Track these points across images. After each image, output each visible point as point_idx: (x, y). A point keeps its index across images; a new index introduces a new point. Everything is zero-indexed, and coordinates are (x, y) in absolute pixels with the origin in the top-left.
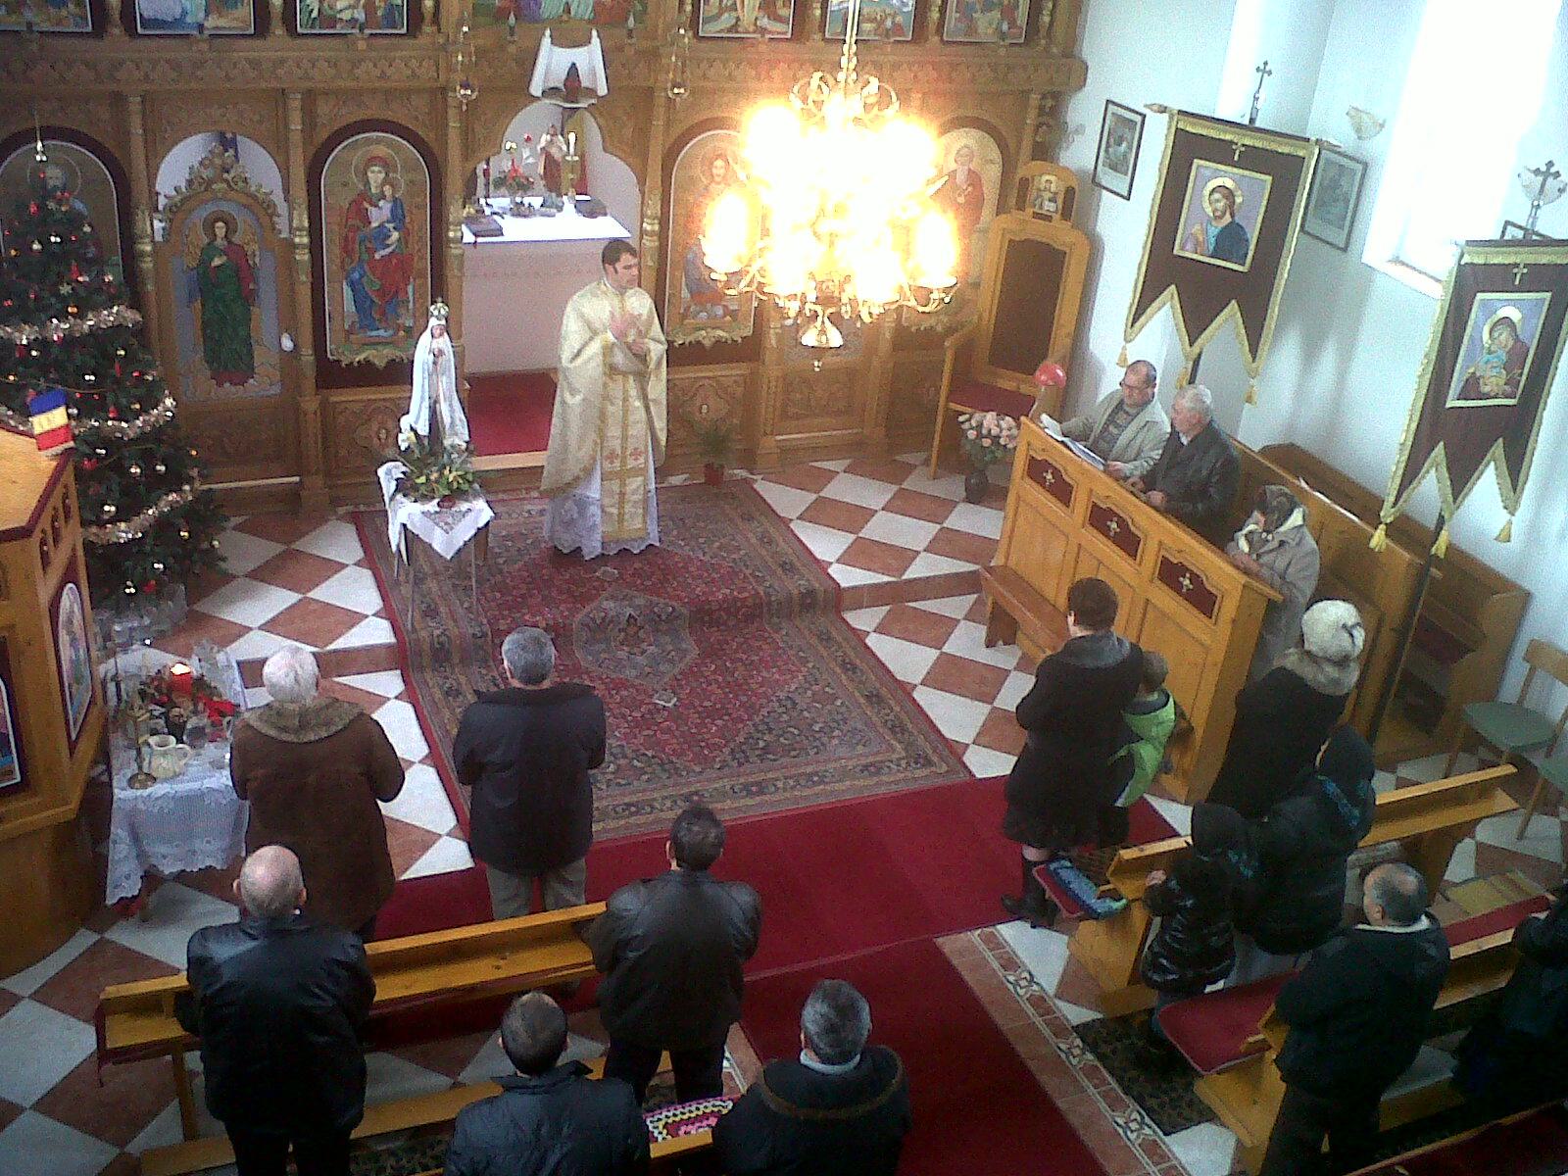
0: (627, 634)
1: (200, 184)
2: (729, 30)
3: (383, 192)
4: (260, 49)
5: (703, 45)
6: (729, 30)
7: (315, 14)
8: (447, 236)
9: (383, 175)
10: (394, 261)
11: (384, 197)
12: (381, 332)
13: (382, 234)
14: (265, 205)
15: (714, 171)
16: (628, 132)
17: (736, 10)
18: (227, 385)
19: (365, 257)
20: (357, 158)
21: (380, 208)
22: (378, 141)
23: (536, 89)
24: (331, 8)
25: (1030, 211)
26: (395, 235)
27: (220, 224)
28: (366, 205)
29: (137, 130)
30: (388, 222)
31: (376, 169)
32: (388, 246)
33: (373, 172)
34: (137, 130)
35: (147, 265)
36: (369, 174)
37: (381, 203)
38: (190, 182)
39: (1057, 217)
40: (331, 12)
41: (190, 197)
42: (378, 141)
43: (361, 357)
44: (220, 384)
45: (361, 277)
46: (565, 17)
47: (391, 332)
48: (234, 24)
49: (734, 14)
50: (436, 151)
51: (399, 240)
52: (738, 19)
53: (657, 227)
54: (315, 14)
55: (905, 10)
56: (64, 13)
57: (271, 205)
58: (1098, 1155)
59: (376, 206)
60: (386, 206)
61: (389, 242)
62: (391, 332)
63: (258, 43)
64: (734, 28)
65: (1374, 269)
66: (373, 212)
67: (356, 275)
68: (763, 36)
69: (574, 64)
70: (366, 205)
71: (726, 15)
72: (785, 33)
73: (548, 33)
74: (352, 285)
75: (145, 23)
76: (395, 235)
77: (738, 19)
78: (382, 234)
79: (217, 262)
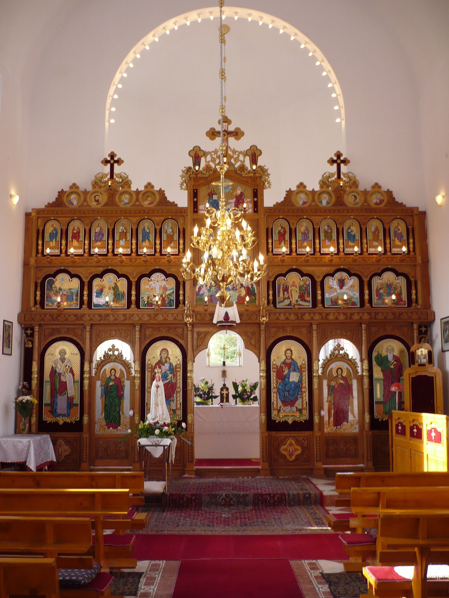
0: (226, 502)
1: (107, 357)
2: (288, 305)
3: (166, 360)
4: (129, 311)
6: (288, 305)
10: (170, 385)
11: (166, 362)
16: (253, 342)
18: (111, 428)
25: (417, 364)
29: (88, 336)
30: (168, 371)
31: (164, 352)
35: (315, 381)
38: (104, 356)
39: (427, 364)
40: (151, 302)
44: (109, 428)
48: (121, 306)
49: (289, 300)
50: (184, 347)
52: (291, 302)
54: (146, 302)
55: (355, 296)
56: (72, 303)
58: (298, 577)
59: (164, 365)
61: (168, 378)
64: (290, 304)
65: (221, 26)
75: (95, 305)
76: (170, 376)
77: (291, 302)
79: (111, 384)
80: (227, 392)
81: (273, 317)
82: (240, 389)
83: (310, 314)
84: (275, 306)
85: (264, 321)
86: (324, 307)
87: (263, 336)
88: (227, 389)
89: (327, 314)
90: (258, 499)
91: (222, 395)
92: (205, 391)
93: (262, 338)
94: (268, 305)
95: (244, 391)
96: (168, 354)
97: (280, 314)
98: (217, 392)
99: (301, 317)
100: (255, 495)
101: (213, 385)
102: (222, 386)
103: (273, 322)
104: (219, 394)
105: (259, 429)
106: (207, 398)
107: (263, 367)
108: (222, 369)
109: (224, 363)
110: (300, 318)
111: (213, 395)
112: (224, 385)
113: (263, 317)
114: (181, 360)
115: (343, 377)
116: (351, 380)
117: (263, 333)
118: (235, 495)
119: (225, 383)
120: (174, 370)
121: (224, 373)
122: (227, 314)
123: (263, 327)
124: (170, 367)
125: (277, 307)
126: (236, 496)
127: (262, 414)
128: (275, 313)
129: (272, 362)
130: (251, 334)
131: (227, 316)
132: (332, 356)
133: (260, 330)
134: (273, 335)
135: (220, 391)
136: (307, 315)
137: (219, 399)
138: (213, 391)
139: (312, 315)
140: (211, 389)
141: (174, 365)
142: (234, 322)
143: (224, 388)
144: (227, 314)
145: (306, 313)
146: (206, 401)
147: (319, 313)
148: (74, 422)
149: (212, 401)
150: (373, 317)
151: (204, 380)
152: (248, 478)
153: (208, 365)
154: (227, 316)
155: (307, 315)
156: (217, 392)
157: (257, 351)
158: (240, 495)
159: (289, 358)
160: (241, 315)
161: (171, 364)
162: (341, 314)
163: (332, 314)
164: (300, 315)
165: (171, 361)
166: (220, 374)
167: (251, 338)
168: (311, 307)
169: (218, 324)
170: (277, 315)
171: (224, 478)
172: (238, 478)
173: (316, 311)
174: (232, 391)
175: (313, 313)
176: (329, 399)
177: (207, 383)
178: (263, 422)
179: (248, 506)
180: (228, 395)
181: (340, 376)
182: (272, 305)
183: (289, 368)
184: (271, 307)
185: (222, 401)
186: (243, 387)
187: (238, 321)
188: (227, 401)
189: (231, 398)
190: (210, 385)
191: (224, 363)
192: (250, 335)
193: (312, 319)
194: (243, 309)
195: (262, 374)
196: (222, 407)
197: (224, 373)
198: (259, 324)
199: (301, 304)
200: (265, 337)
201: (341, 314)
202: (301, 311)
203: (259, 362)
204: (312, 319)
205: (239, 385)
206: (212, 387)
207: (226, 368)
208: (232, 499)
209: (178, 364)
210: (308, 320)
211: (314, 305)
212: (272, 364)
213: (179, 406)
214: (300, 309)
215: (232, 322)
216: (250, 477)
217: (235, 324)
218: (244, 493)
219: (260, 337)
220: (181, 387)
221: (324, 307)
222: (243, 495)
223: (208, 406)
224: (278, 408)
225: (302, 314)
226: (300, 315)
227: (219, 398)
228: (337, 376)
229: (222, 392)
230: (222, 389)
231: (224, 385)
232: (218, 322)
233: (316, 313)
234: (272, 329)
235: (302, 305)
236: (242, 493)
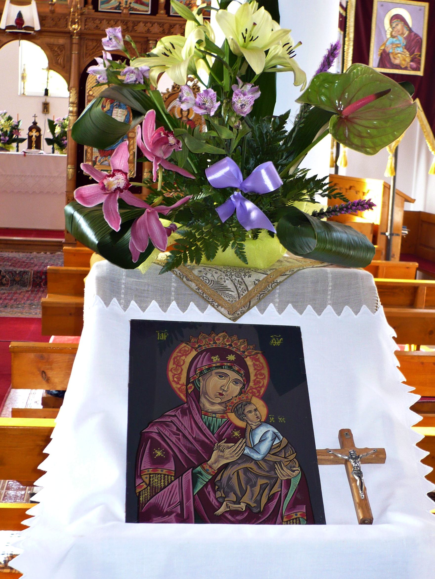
2: (115, 8)
6: (115, 8)
16: (61, 60)
41: (173, 94)
72: (147, 11)
80: (37, 134)
81: (91, 25)
82: (58, 130)
83: (145, 23)
84: (96, 8)
85: (74, 29)
86: (169, 15)
87: (75, 53)
88: (39, 130)
89: (171, 26)
90: (41, 278)
91: (30, 137)
92: (5, 130)
93: (73, 55)
94: (85, 6)
95: (64, 133)
97: (101, 20)
98: (24, 134)
99: (133, 27)
100: (36, 273)
101: (19, 122)
102: (32, 124)
103: (90, 32)
104: (26, 137)
105: (65, 186)
106: (8, 141)
107: (74, 98)
108: (43, 100)
109: (46, 91)
110: (130, 29)
111: (19, 137)
112: (35, 123)
113: (73, 23)
115: (189, 120)
116: (201, 124)
117: (75, 47)
118: (9, 272)
119: (37, 121)
121: (46, 107)
122: (20, 15)
123: (76, 38)
125: (100, 10)
126: (10, 272)
127: (69, 166)
128: (94, 19)
129: (87, 91)
130: (59, 48)
131: (20, 18)
132: (176, 89)
133: (72, 44)
134: (91, 52)
135: (28, 131)
136: (141, 24)
137: (26, 143)
138: (20, 131)
139: (149, 25)
140: (15, 128)
142: (32, 29)
143: (35, 127)
144: (20, 15)
145: (139, 22)
146: (7, 146)
147: (159, 24)
149: (18, 146)
150: (130, 29)
151: (5, 114)
152: (46, 253)
153: (23, 92)
154: (20, 18)
155: (141, 24)
156: (24, 134)
157: (68, 75)
158: (15, 272)
160: (42, 18)
162: (156, 24)
163: (177, 26)
164: (130, 24)
166: (40, 107)
167: (59, 55)
168: (149, 13)
169: (7, 31)
170: (98, 22)
171: (12, 252)
172: (31, 253)
173: (154, 21)
174: (47, 134)
175: (151, 22)
177: (10, 118)
178: (70, 178)
179: (26, 286)
180: (39, 138)
181: (184, 119)
182: (91, 7)
184: (89, 9)
185: (30, 147)
186: (63, 127)
187: (37, 27)
188: (38, 147)
189: (44, 143)
190: (14, 122)
191: (46, 91)
192: (56, 49)
193: (148, 31)
194: (47, 10)
195: (71, 109)
196: (25, 155)
197: (46, 107)
198: (70, 34)
199: (135, 7)
200: (79, 54)
201: (156, 24)
202: (133, 18)
203: (69, 90)
204: (148, 31)
205: (56, 125)
206: (17, 126)
207: (48, 100)
208: (4, 277)
210: (143, 33)
211: (155, 11)
212: (87, 95)
214: (133, 16)
215: (28, 28)
216: (48, 253)
217: (32, 32)
218: (22, 270)
219: (71, 54)
221: (169, 15)
222: (21, 271)
223: (8, 153)
224: (94, 159)
225: (133, 22)
226: (130, 24)
227: (26, 142)
228: (181, 118)
229: (31, 134)
230: (30, 129)
231: (35, 123)
232: (8, 27)
233: (154, 23)
234: (90, 43)
235: (136, 10)
236: (19, 270)
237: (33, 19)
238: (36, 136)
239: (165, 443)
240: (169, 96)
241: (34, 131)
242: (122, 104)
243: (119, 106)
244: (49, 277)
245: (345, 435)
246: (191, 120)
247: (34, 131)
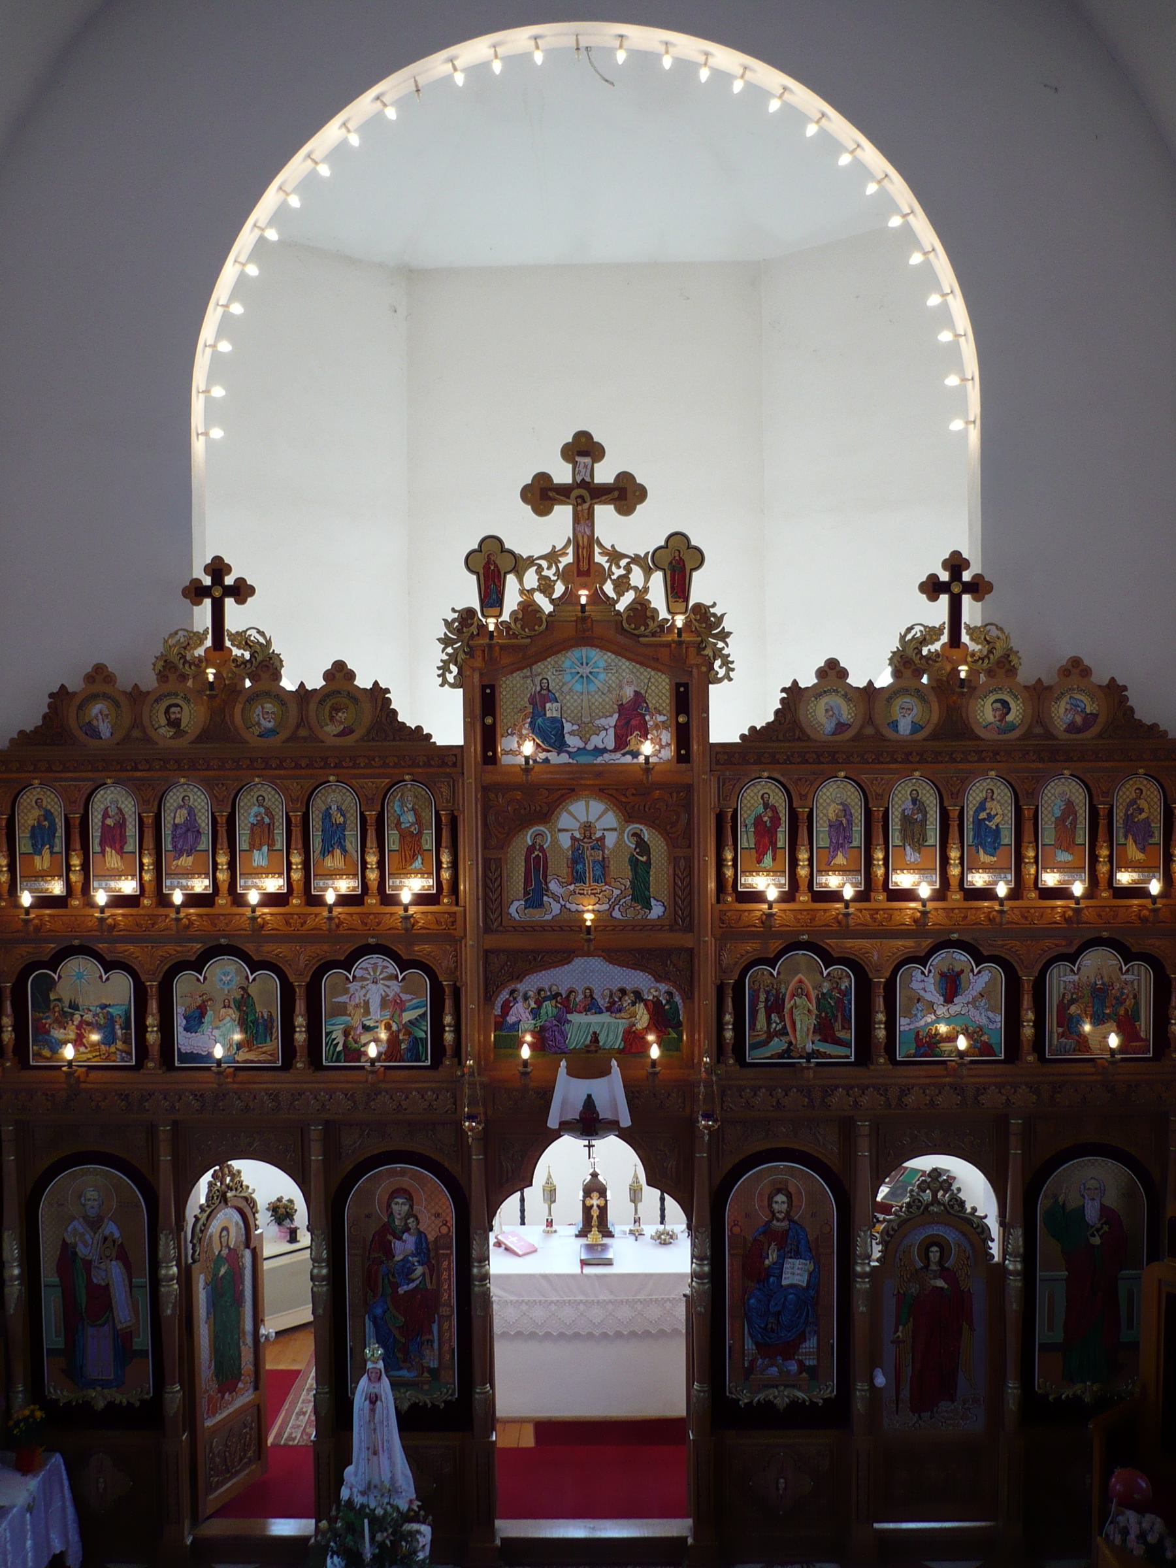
2: (780, 1056)
3: (406, 1224)
5: (750, 1072)
6: (780, 1056)
7: (340, 1048)
8: (854, 1269)
9: (406, 1208)
12: (404, 1373)
13: (406, 1271)
14: (979, 1230)
15: (775, 1206)
17: (787, 1034)
19: (389, 1291)
20: (381, 1192)
21: (405, 1241)
22: (403, 1173)
23: (553, 1123)
24: (356, 1042)
26: (419, 1270)
27: (934, 1249)
28: (390, 1237)
29: (165, 1158)
30: (413, 1255)
31: (400, 1201)
32: (413, 1281)
33: (397, 1203)
34: (165, 1158)
35: (862, 1285)
36: (394, 1206)
37: (405, 1236)
41: (909, 1220)
42: (403, 1173)
43: (761, 1396)
45: (385, 1312)
46: (593, 1048)
47: (414, 1374)
48: (262, 1057)
51: (424, 1274)
53: (1019, 1267)
54: (340, 1048)
56: (113, 1049)
57: (985, 1230)
59: (400, 1239)
60: (410, 1240)
61: (413, 1276)
62: (414, 1374)
63: (283, 1075)
64: (787, 1053)
66: (397, 1246)
67: (379, 1311)
68: (808, 1061)
69: (589, 1096)
70: (390, 1237)
71: (776, 1039)
72: (848, 1057)
73: (563, 1063)
74: (375, 1321)
75: (184, 1057)
78: (406, 1271)
80: (601, 1202)
96: (411, 1207)
114: (452, 1223)
119: (598, 1170)
120: (432, 1254)
122: (589, 1103)
124: (418, 1245)
141: (431, 1238)
144: (589, 1103)
148: (138, 1404)
159: (780, 1216)
161: (421, 1235)
165: (422, 1228)
176: (899, 1334)
183: (780, 1248)
209: (443, 1236)
213: (447, 1357)
220: (454, 1302)
229: (588, 1202)
233: (867, 1087)
235: (825, 1055)
237: (615, 1107)
238: (598, 1206)
239: (674, 860)
240: (900, 1225)
241: (595, 1195)
242: (802, 1248)
243: (797, 1255)
244: (486, 683)
245: (932, 588)
246: (948, 1269)
247: (595, 1195)
